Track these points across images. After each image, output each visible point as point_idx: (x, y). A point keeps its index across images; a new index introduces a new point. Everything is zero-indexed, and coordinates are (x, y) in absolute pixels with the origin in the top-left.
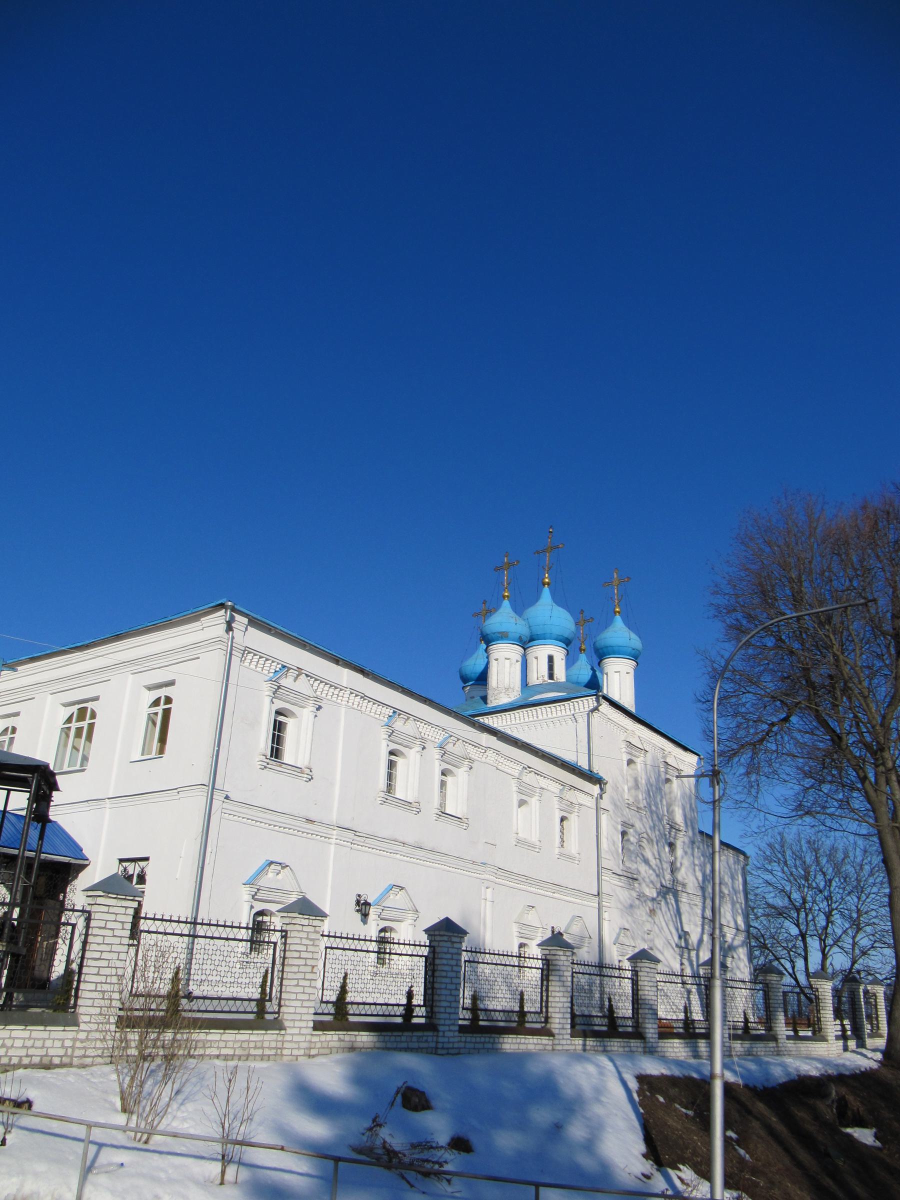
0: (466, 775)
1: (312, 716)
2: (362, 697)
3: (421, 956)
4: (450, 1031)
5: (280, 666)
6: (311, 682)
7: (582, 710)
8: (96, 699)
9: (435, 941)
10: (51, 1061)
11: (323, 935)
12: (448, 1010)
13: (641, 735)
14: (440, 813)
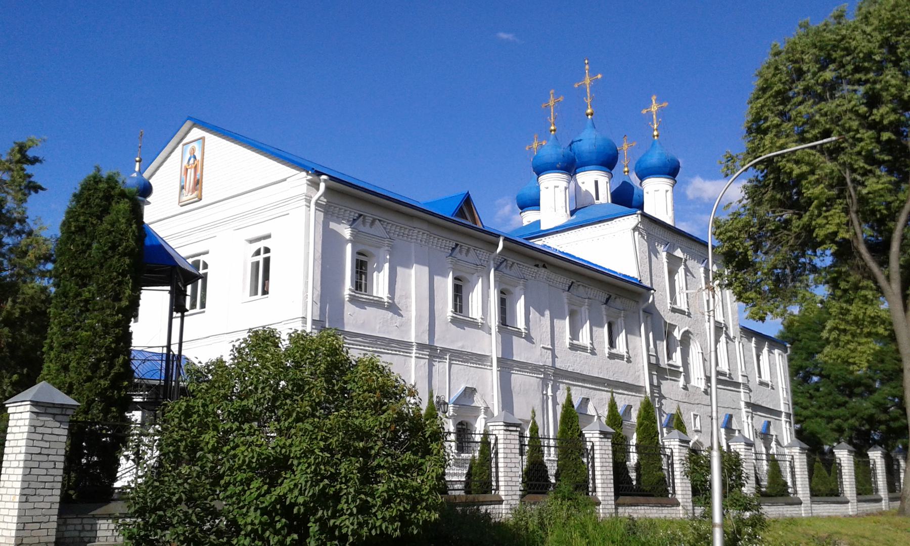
5: (357, 215)
8: (207, 253)
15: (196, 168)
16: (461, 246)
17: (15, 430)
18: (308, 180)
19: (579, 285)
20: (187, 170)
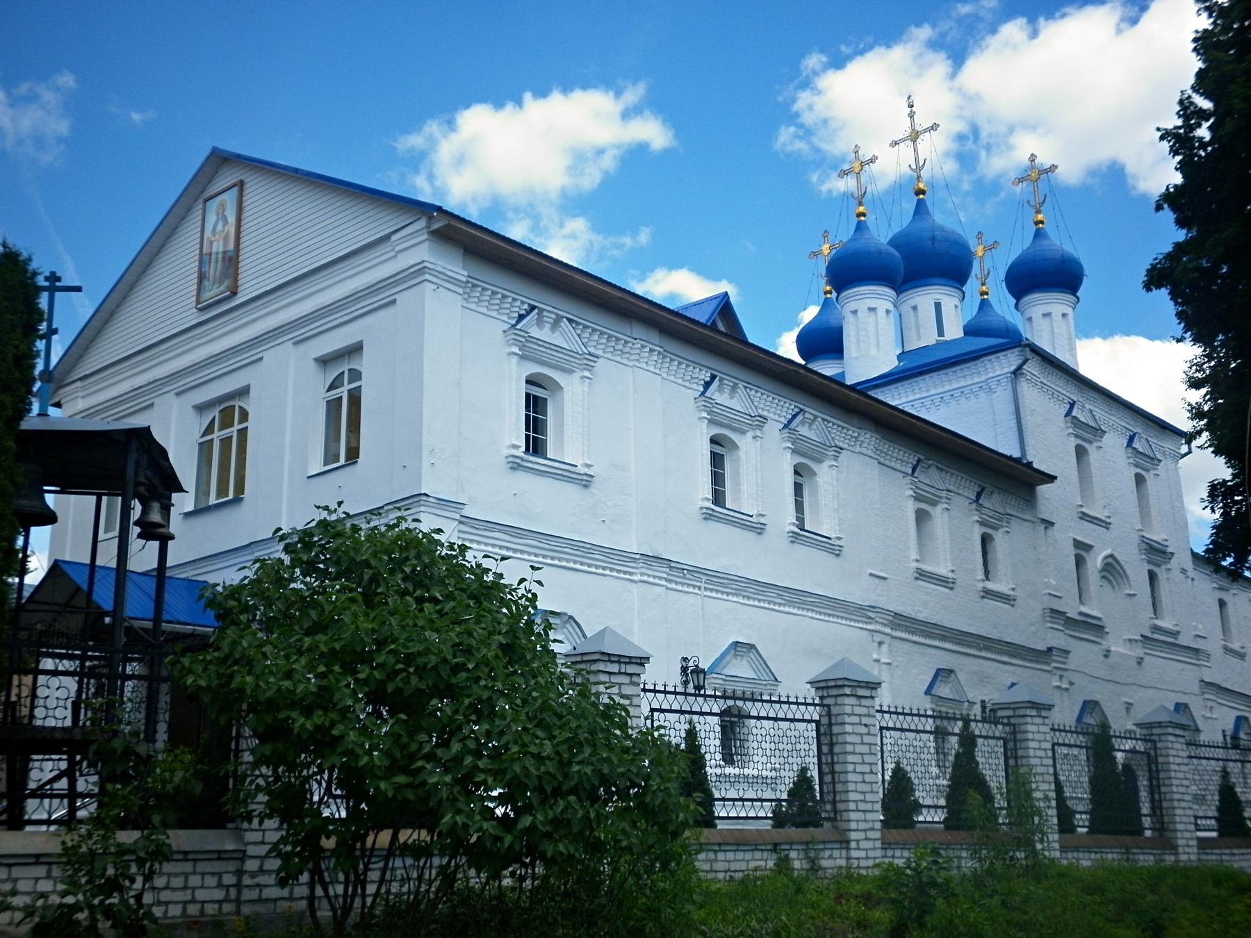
2: (659, 353)
3: (809, 721)
4: (867, 839)
9: (829, 696)
10: (202, 911)
11: (644, 690)
12: (862, 806)
16: (721, 380)
19: (929, 466)
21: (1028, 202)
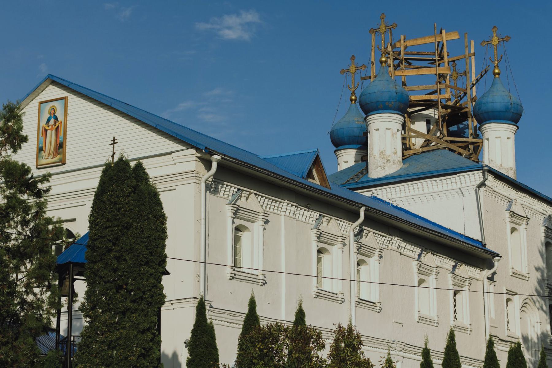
0: (377, 263)
1: (261, 228)
2: (296, 206)
6: (259, 199)
7: (468, 184)
13: (523, 203)
14: (359, 301)
15: (57, 129)
17: (472, 176)
18: (197, 157)
20: (46, 131)
21: (349, 86)
